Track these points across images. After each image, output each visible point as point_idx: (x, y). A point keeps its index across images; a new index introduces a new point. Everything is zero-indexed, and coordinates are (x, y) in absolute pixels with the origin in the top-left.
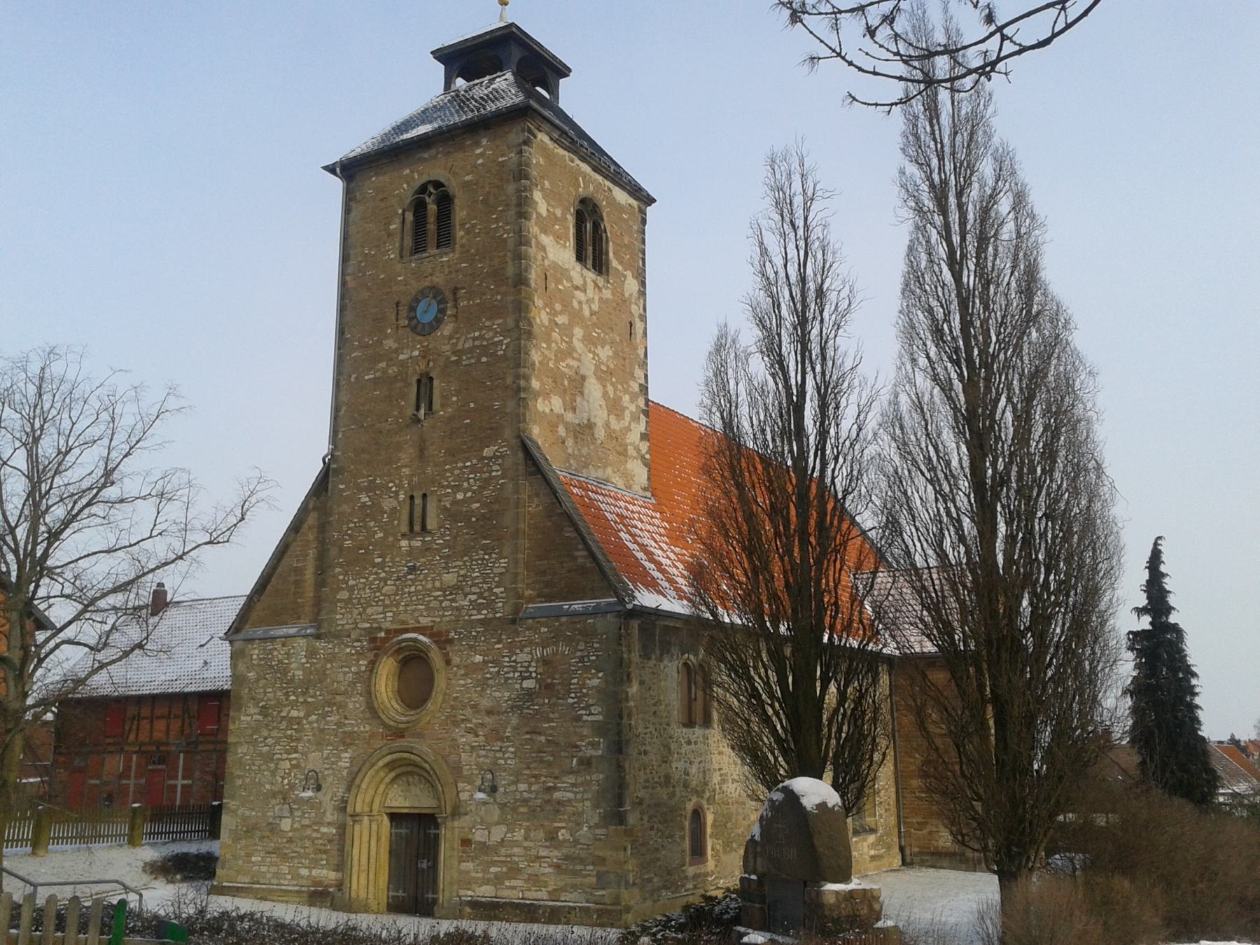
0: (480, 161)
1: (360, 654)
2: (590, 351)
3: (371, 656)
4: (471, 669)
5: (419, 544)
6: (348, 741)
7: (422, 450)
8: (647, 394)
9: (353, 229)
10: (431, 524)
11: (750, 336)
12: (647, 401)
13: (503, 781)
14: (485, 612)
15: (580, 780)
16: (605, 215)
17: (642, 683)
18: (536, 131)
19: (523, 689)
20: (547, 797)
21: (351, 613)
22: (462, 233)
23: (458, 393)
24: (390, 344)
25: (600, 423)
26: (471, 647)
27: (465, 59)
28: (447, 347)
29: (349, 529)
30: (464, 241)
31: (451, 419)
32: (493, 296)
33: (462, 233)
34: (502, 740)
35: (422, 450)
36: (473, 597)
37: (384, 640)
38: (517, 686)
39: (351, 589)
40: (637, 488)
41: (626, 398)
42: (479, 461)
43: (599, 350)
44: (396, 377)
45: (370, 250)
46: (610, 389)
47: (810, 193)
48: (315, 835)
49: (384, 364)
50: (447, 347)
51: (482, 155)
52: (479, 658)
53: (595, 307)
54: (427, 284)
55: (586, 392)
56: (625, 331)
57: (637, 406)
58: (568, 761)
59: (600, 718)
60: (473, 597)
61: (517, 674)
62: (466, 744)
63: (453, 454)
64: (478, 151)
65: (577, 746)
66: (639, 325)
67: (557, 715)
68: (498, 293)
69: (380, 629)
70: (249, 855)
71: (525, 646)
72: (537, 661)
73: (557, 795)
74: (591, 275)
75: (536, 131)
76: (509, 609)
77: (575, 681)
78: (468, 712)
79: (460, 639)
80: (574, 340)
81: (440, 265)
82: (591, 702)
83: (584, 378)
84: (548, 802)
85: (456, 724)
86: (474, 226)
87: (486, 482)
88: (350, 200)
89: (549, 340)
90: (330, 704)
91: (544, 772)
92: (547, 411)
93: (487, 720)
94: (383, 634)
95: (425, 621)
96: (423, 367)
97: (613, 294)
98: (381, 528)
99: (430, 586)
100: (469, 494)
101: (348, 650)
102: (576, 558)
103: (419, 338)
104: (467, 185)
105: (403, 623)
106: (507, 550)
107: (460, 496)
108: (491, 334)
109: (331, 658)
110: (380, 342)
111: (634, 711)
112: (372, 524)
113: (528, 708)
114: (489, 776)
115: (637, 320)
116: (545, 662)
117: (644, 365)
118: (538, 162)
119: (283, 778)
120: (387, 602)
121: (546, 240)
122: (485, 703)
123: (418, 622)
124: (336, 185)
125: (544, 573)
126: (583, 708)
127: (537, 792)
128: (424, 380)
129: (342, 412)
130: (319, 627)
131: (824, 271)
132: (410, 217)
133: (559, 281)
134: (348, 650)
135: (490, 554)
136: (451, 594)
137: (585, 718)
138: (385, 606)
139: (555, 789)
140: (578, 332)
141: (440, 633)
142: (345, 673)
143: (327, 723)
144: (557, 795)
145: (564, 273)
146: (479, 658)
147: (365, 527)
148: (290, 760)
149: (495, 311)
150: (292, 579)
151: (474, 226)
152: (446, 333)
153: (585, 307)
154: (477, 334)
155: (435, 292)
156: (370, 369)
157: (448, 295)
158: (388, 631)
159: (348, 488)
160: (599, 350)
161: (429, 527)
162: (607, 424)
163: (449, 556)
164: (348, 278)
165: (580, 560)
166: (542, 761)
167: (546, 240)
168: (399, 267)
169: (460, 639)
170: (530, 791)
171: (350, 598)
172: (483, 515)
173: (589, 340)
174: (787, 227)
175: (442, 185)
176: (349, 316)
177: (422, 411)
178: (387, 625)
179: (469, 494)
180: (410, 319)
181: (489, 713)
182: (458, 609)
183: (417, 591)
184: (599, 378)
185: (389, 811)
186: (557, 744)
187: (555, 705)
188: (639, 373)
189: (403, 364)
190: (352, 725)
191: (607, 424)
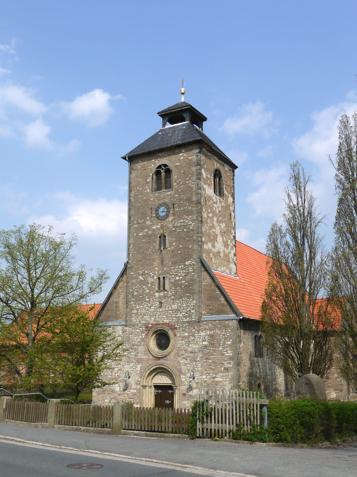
0: (182, 158)
1: (142, 332)
2: (219, 226)
3: (146, 332)
4: (183, 338)
5: (162, 294)
6: (139, 361)
7: (162, 262)
8: (235, 239)
9: (132, 181)
10: (167, 287)
11: (285, 226)
12: (235, 241)
13: (197, 375)
14: (188, 318)
15: (224, 374)
16: (222, 175)
17: (244, 343)
18: (202, 148)
19: (203, 345)
20: (213, 380)
21: (138, 318)
22: (175, 184)
23: (175, 242)
24: (148, 223)
25: (221, 251)
26: (183, 330)
27: (172, 115)
28: (171, 225)
29: (136, 288)
30: (176, 187)
31: (173, 251)
32: (188, 207)
33: (175, 184)
34: (196, 361)
35: (162, 262)
36: (184, 313)
37: (151, 328)
38: (201, 344)
39: (137, 310)
40: (233, 273)
41: (229, 241)
42: (184, 266)
43: (221, 225)
44: (151, 235)
45: (140, 188)
46: (225, 238)
47: (306, 179)
48: (128, 393)
49: (146, 230)
50: (171, 225)
51: (182, 156)
52: (186, 334)
53: (220, 209)
54: (162, 202)
55: (218, 240)
56: (228, 217)
57: (233, 244)
58: (220, 368)
59: (231, 354)
60: (184, 313)
61: (201, 340)
62: (183, 362)
63: (174, 263)
64: (181, 154)
65: (223, 364)
66: (233, 214)
67: (215, 353)
68: (190, 206)
69: (150, 324)
70: (104, 400)
71: (203, 330)
72: (208, 335)
73: (216, 379)
74: (218, 198)
75: (202, 148)
76: (197, 317)
77: (222, 342)
78: (183, 352)
79: (180, 328)
80: (214, 222)
81: (166, 195)
82: (228, 349)
83: (217, 235)
84: (213, 382)
85: (179, 356)
86: (180, 182)
87: (187, 274)
88: (131, 169)
89: (207, 223)
90: (131, 348)
91: (212, 372)
92: (207, 248)
93: (190, 355)
94: (150, 325)
95: (166, 321)
96: (162, 231)
97: (225, 204)
98: (148, 288)
99: (167, 309)
100: (181, 278)
101: (138, 331)
102: (221, 301)
103: (160, 221)
104: (177, 167)
105: (158, 322)
106: (196, 298)
107: (177, 278)
108: (187, 221)
109: (131, 333)
110: (145, 222)
111: (242, 352)
112: (144, 287)
113: (205, 351)
114: (192, 373)
115: (232, 212)
116: (211, 336)
117: (234, 228)
118: (203, 159)
119: (115, 374)
120: (151, 314)
121: (206, 187)
122: (190, 349)
123: (164, 322)
124: (126, 163)
125: (209, 306)
126: (225, 351)
127: (209, 379)
128: (162, 236)
129: (131, 247)
130: (126, 322)
131: (311, 206)
132: (155, 177)
133: (209, 201)
134: (138, 331)
135: (189, 299)
136: (175, 312)
137: (226, 354)
138: (151, 316)
139: (216, 377)
140: (215, 219)
141: (172, 325)
142: (137, 338)
143: (131, 355)
144: (216, 379)
145: (210, 198)
146: (186, 334)
147: (142, 288)
148: (118, 367)
149: (189, 213)
150: (114, 305)
151: (180, 182)
152: (170, 220)
153: (217, 209)
154: (182, 221)
155: (164, 204)
156: (141, 232)
157: (171, 206)
158: (152, 324)
159: (134, 274)
160: (221, 225)
161: (166, 289)
162: (224, 251)
163: (174, 299)
164: (131, 198)
165: (223, 302)
166: (210, 368)
167: (206, 187)
168: (151, 195)
169: (180, 328)
170: (206, 378)
171: (137, 313)
172: (186, 285)
173: (219, 222)
174: (298, 191)
175: (167, 166)
176: (132, 212)
177: (162, 248)
178: (152, 322)
179: (181, 278)
180: (156, 214)
181: (191, 352)
182: (178, 317)
183: (162, 311)
184: (222, 235)
185: (154, 385)
186: (216, 363)
187: (215, 350)
188: (233, 231)
189: (154, 230)
190: (140, 356)
191: (224, 251)
